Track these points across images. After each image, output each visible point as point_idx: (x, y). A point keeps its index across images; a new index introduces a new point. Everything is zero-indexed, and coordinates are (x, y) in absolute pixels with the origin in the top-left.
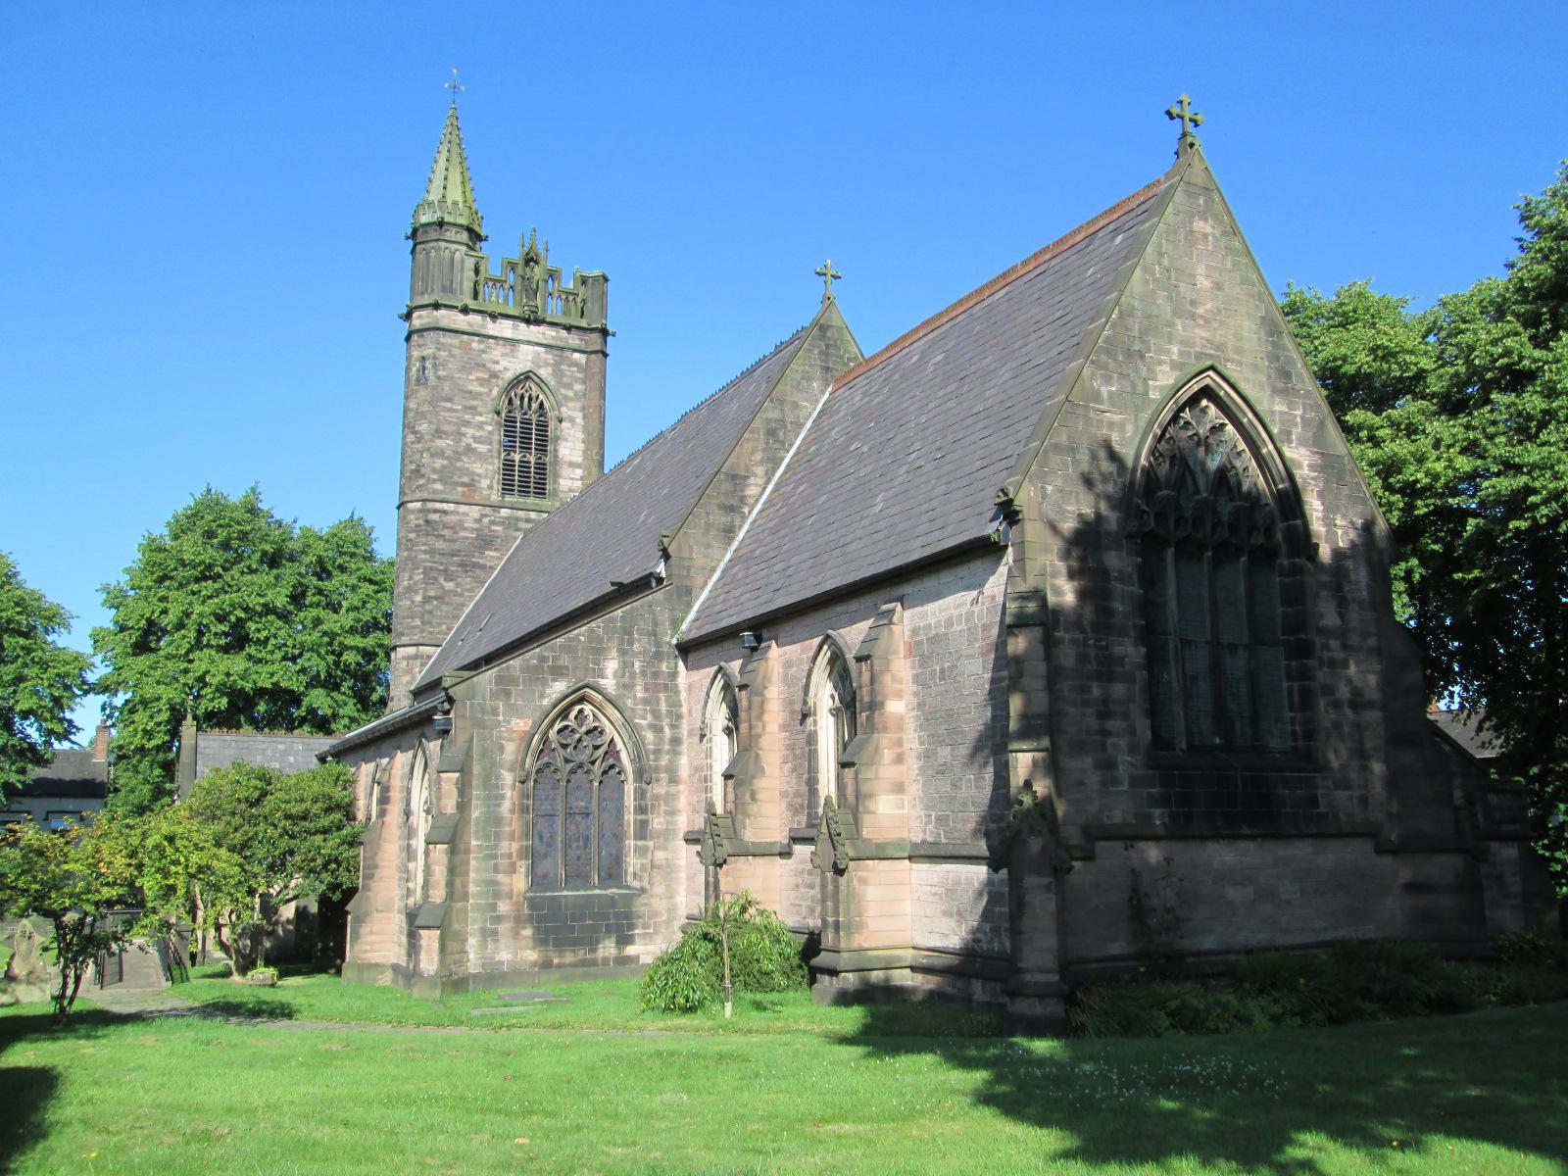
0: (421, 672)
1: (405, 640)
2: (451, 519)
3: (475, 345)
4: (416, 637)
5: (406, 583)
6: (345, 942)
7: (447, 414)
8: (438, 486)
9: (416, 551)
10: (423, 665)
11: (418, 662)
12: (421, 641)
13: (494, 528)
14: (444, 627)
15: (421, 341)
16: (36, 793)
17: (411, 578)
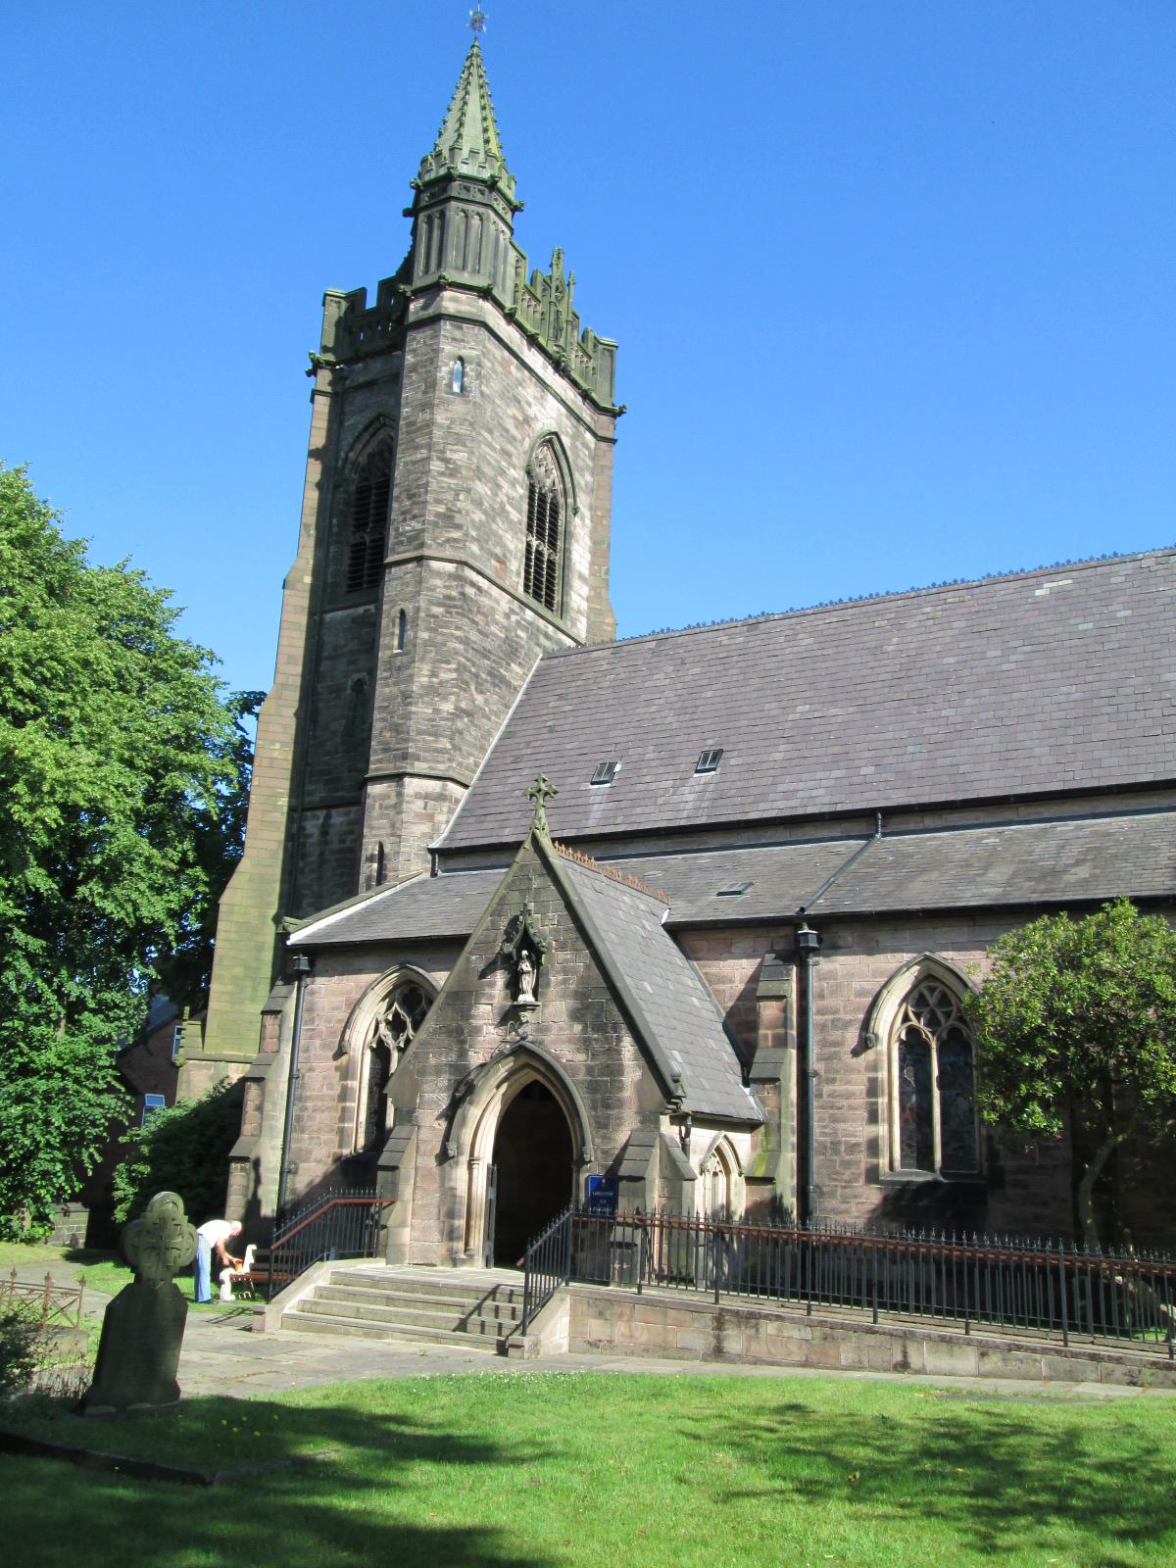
0: (448, 822)
1: (420, 767)
2: (484, 600)
3: (513, 369)
4: (441, 766)
5: (425, 679)
6: (570, 1133)
7: (488, 450)
8: (475, 548)
9: (443, 634)
10: (451, 811)
11: (445, 807)
12: (450, 774)
13: (520, 632)
14: (472, 760)
15: (457, 334)
16: (312, 826)
17: (434, 674)
